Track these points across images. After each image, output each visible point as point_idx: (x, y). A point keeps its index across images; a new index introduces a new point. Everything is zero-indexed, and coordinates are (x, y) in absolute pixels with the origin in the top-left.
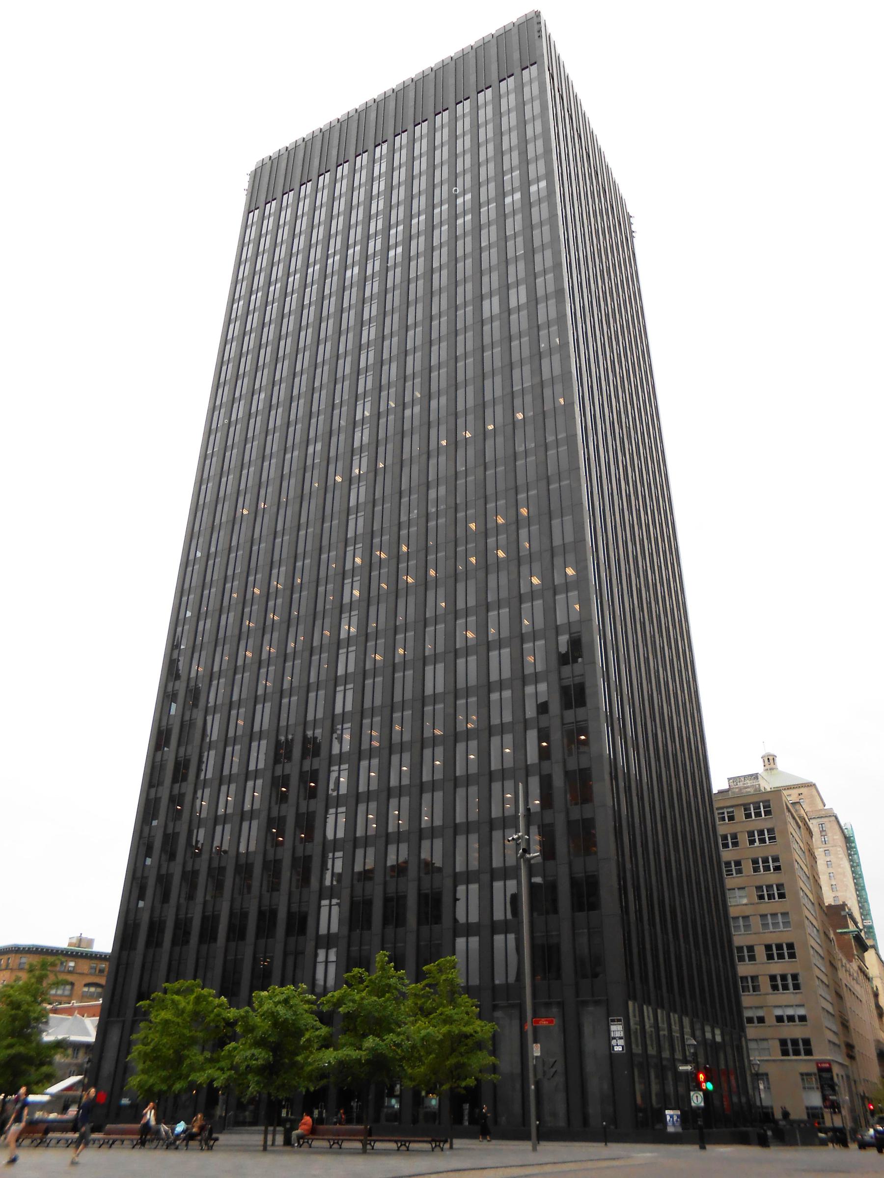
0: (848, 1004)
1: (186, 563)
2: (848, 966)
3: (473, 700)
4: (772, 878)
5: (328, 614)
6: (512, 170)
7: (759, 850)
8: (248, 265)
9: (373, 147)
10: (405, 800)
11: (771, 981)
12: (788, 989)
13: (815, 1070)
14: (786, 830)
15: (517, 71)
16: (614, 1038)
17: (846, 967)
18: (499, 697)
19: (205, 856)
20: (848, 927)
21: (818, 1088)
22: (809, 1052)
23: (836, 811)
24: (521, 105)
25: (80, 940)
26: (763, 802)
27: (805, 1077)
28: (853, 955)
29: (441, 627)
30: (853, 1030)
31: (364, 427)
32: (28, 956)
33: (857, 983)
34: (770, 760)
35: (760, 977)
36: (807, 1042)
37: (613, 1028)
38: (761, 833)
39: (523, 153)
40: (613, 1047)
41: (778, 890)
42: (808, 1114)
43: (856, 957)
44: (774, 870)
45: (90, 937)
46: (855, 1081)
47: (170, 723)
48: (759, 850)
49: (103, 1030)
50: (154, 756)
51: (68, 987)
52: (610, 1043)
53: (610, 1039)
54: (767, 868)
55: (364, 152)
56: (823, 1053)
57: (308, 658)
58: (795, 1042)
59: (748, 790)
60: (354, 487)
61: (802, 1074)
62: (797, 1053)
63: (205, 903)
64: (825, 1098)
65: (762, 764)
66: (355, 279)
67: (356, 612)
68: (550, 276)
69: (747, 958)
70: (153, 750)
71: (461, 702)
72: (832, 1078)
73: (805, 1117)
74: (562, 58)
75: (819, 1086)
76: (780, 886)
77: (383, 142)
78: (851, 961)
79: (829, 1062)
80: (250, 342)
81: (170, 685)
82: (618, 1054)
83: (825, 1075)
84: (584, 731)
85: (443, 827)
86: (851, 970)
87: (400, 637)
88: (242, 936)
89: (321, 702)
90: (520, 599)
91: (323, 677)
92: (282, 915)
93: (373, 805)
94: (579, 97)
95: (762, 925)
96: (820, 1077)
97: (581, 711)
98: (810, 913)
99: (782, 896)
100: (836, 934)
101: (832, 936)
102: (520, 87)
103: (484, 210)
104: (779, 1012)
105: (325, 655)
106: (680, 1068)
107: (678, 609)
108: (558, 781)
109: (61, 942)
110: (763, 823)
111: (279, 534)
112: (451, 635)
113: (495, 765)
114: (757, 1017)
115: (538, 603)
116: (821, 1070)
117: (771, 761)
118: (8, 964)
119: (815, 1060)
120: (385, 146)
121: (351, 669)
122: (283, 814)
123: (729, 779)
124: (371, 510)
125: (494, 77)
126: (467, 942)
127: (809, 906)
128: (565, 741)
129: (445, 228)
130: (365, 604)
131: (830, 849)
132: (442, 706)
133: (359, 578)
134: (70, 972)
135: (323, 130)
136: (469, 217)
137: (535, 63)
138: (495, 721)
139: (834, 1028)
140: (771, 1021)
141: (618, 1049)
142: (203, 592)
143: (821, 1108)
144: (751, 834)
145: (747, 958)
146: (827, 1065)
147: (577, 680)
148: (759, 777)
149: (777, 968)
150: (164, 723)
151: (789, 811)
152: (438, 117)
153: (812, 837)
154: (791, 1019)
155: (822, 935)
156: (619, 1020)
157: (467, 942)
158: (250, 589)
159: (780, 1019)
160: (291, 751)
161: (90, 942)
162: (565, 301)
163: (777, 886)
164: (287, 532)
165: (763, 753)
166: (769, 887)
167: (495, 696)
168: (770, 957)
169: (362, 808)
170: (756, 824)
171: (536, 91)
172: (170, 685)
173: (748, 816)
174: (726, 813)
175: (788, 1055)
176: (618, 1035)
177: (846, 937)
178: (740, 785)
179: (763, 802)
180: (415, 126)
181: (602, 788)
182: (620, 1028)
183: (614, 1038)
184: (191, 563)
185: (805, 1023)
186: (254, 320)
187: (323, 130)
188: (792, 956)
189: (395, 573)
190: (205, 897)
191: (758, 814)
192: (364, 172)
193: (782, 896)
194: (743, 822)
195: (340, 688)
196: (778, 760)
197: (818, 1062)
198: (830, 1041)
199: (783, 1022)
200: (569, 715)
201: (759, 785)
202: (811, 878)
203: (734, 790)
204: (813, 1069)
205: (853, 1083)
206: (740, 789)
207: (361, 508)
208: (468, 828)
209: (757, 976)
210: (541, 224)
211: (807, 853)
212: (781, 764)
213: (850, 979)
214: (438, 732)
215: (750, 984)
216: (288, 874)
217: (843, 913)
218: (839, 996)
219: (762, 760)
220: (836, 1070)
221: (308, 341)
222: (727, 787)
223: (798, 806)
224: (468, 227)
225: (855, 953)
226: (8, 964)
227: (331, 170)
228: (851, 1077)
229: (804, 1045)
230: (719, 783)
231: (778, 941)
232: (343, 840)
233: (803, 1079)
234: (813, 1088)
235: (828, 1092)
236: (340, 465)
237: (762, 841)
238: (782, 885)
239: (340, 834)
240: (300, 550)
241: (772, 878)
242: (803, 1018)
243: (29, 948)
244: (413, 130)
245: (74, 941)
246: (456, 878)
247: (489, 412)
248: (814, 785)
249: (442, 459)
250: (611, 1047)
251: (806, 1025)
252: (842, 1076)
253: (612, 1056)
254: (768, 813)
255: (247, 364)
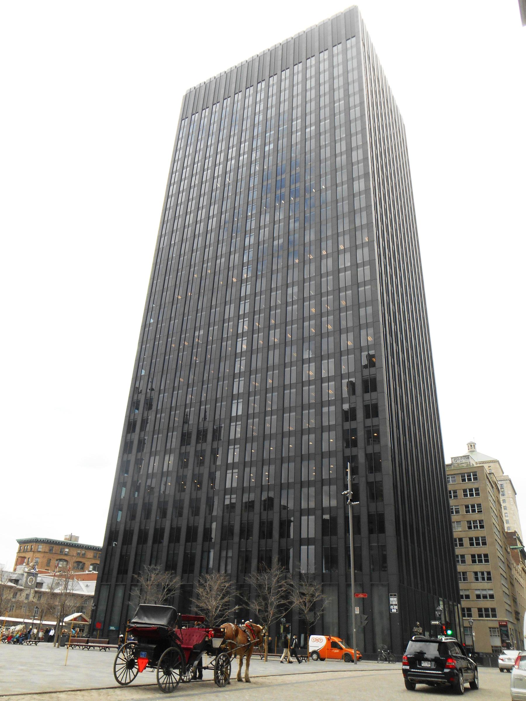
0: (517, 590)
1: (145, 325)
2: (517, 568)
3: (312, 411)
4: (476, 516)
5: (228, 358)
6: (339, 100)
7: (470, 501)
8: (181, 151)
9: (257, 83)
10: (272, 467)
11: (491, 577)
12: (485, 580)
13: (498, 626)
14: (486, 489)
15: (343, 41)
16: (392, 605)
17: (515, 568)
18: (328, 411)
19: (156, 494)
20: (517, 545)
21: (499, 636)
22: (494, 616)
23: (510, 477)
24: (346, 61)
25: (71, 536)
26: (472, 472)
27: (492, 630)
28: (519, 561)
29: (294, 368)
30: (518, 604)
31: (250, 250)
32: (43, 544)
33: (521, 577)
34: (472, 446)
35: (467, 573)
36: (493, 610)
37: (391, 599)
38: (471, 490)
39: (347, 91)
40: (391, 609)
41: (480, 523)
42: (493, 650)
43: (521, 562)
44: (478, 512)
45: (77, 535)
46: (519, 633)
47: (135, 418)
48: (470, 501)
49: (98, 589)
50: (126, 437)
51: (65, 563)
52: (389, 607)
53: (389, 605)
54: (474, 511)
55: (251, 87)
56: (502, 616)
57: (216, 383)
58: (487, 610)
59: (463, 465)
60: (244, 285)
61: (490, 628)
62: (487, 616)
63: (156, 521)
64: (503, 641)
65: (467, 448)
66: (245, 162)
67: (244, 358)
68: (361, 165)
69: (460, 561)
70: (125, 433)
71: (305, 412)
72: (507, 631)
73: (491, 652)
74: (369, 34)
75: (500, 635)
76: (481, 521)
77: (263, 81)
78: (518, 565)
79: (506, 622)
80: (183, 197)
81: (136, 396)
82: (394, 614)
83: (503, 629)
84: (378, 432)
85: (294, 483)
86: (519, 570)
87: (270, 373)
88: (178, 540)
89: (224, 409)
90: (341, 354)
91: (225, 394)
92: (201, 530)
93: (254, 469)
94: (378, 56)
95: (470, 543)
96: (501, 630)
97: (375, 420)
98: (498, 537)
99: (482, 527)
100: (510, 548)
101: (509, 550)
102: (345, 51)
103: (322, 124)
104: (478, 592)
105: (226, 382)
106: (433, 623)
107: (428, 360)
108: (362, 459)
109: (61, 537)
110: (472, 485)
111: (200, 311)
112: (300, 373)
113: (325, 448)
114: (465, 595)
115: (351, 357)
116: (501, 626)
117: (473, 447)
118: (31, 549)
119: (497, 620)
120: (263, 83)
121: (241, 391)
122: (201, 472)
123: (452, 458)
124: (254, 299)
125: (330, 44)
126: (308, 548)
127: (497, 533)
128: (366, 436)
129: (299, 134)
130: (249, 353)
131: (506, 499)
132: (294, 414)
133: (246, 338)
134: (66, 555)
135: (227, 72)
136: (313, 128)
137: (354, 36)
138: (325, 423)
139: (509, 603)
140: (473, 597)
141: (394, 611)
142: (154, 343)
143: (500, 647)
144: (465, 491)
145: (460, 561)
146: (505, 623)
147: (374, 402)
148: (470, 458)
149: (478, 567)
150: (132, 417)
151: (488, 478)
152: (296, 67)
153: (499, 493)
154: (485, 597)
155: (504, 550)
156: (395, 595)
157: (308, 548)
158: (182, 342)
159: (478, 597)
160: (206, 437)
161: (77, 538)
162: (370, 180)
163: (479, 521)
164: (204, 310)
165: (469, 441)
166: (475, 522)
167: (325, 410)
168: (474, 561)
169: (247, 470)
170: (468, 485)
171: (355, 54)
172: (136, 396)
173: (464, 480)
174: (450, 478)
175: (483, 617)
176: (394, 603)
177: (516, 551)
178: (459, 462)
179: (472, 472)
180: (282, 72)
181: (387, 465)
182: (395, 599)
183: (392, 605)
184: (148, 326)
185: (493, 600)
186: (185, 184)
187: (227, 72)
188: (487, 561)
189: (173, 293)
190: (156, 518)
191: (470, 480)
192: (251, 98)
193: (482, 527)
194: (461, 483)
195: (235, 402)
196: (476, 446)
197: (499, 621)
198: (506, 610)
199: (480, 598)
200: (369, 422)
201: (470, 462)
202: (499, 517)
203: (455, 465)
204: (497, 625)
205: (518, 633)
206: (458, 464)
207: (248, 297)
208: (309, 484)
209: (466, 572)
210: (357, 133)
211: (497, 502)
212: (478, 448)
213: (517, 575)
214: (291, 429)
215: (462, 577)
216: (204, 506)
217: (514, 537)
218: (512, 585)
219: (467, 446)
220: (510, 626)
221: (207, 190)
222: (451, 463)
223: (492, 475)
224: (313, 134)
225: (521, 560)
226: (31, 549)
227: (231, 96)
228: (518, 630)
229: (485, 611)
230: (448, 461)
231: (479, 553)
232: (236, 488)
233: (490, 631)
234: (496, 636)
235: (505, 638)
236: (235, 272)
237: (472, 495)
238: (483, 520)
239: (235, 485)
240: (212, 321)
241: (476, 516)
242: (492, 596)
243: (43, 540)
244: (280, 74)
245: (68, 537)
246: (302, 512)
247: (323, 245)
248: (498, 462)
249: (296, 270)
250: (390, 610)
251: (494, 601)
252: (513, 630)
253: (391, 615)
254: (475, 479)
255: (181, 210)
